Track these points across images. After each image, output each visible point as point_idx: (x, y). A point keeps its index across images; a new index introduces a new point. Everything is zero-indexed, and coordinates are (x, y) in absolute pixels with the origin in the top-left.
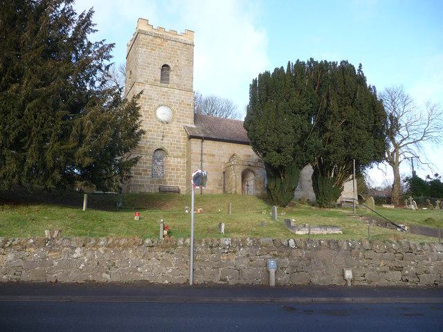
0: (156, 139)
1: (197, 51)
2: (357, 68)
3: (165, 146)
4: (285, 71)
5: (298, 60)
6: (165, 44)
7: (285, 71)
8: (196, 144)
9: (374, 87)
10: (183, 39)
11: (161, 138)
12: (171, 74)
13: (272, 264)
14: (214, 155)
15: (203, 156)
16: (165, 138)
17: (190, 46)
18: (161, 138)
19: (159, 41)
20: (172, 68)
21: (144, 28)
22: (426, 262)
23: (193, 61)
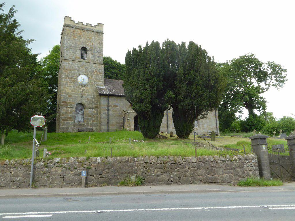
0: (78, 97)
1: (105, 36)
2: (199, 46)
3: (83, 101)
4: (187, 47)
5: (153, 41)
6: (84, 33)
7: (187, 47)
8: (103, 101)
9: (213, 57)
10: (97, 29)
11: (81, 96)
12: (89, 54)
13: (84, 173)
14: (117, 106)
15: (109, 107)
16: (83, 96)
17: (100, 33)
18: (81, 96)
19: (79, 31)
20: (88, 49)
21: (69, 23)
22: (185, 169)
23: (103, 44)
